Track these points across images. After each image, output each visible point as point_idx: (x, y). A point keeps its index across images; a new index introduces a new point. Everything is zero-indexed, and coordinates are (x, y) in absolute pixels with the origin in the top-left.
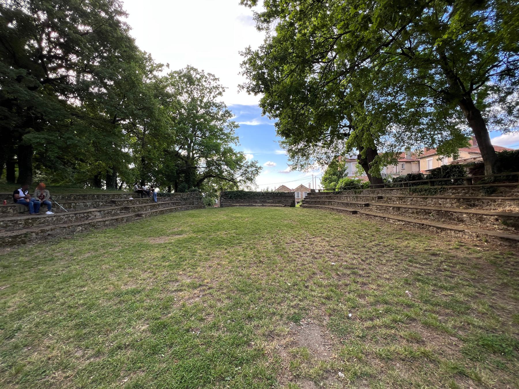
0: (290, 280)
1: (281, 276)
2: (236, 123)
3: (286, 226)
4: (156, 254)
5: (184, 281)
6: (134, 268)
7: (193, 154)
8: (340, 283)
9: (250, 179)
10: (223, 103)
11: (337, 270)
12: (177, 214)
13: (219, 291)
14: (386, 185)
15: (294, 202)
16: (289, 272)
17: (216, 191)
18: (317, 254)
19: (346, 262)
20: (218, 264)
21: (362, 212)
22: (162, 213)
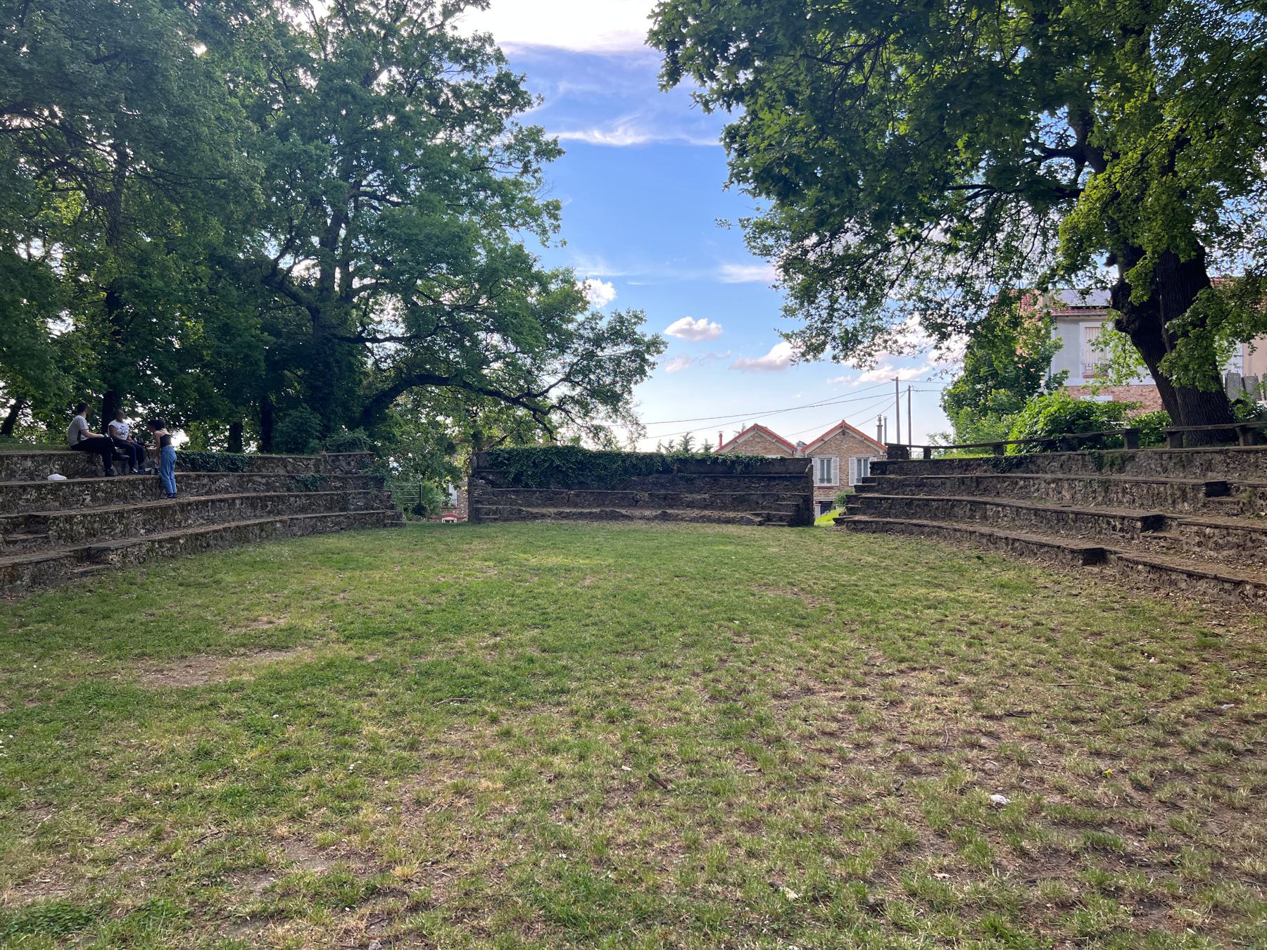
0: (793, 874)
1: (751, 854)
2: (548, 137)
3: (770, 612)
4: (168, 739)
5: (296, 870)
6: (62, 806)
7: (347, 278)
8: (1036, 893)
9: (612, 398)
10: (488, 39)
11: (1019, 829)
12: (272, 549)
13: (459, 920)
14: (1245, 430)
15: (808, 501)
16: (792, 834)
17: (451, 448)
18: (922, 749)
19: (1062, 790)
20: (459, 792)
21: (1132, 554)
22: (200, 544)
